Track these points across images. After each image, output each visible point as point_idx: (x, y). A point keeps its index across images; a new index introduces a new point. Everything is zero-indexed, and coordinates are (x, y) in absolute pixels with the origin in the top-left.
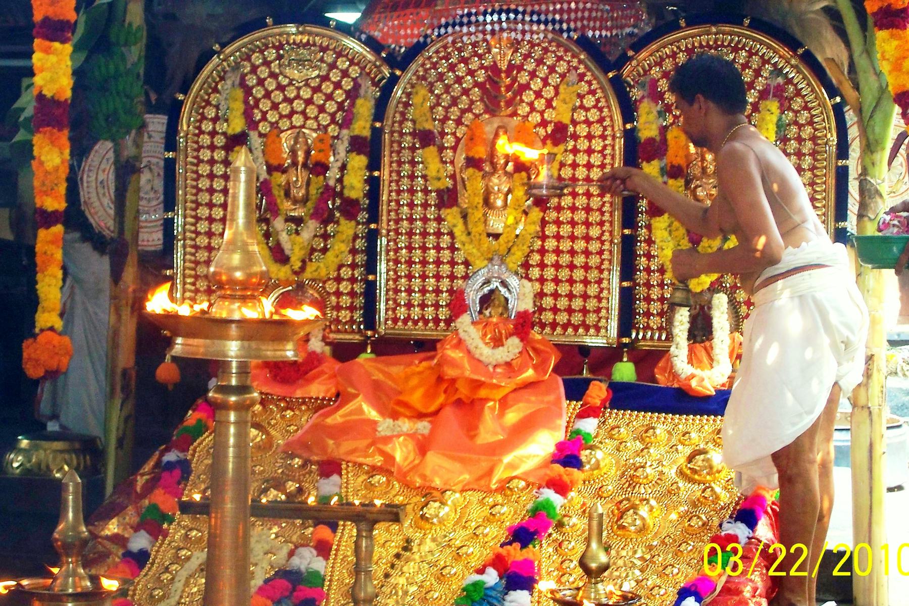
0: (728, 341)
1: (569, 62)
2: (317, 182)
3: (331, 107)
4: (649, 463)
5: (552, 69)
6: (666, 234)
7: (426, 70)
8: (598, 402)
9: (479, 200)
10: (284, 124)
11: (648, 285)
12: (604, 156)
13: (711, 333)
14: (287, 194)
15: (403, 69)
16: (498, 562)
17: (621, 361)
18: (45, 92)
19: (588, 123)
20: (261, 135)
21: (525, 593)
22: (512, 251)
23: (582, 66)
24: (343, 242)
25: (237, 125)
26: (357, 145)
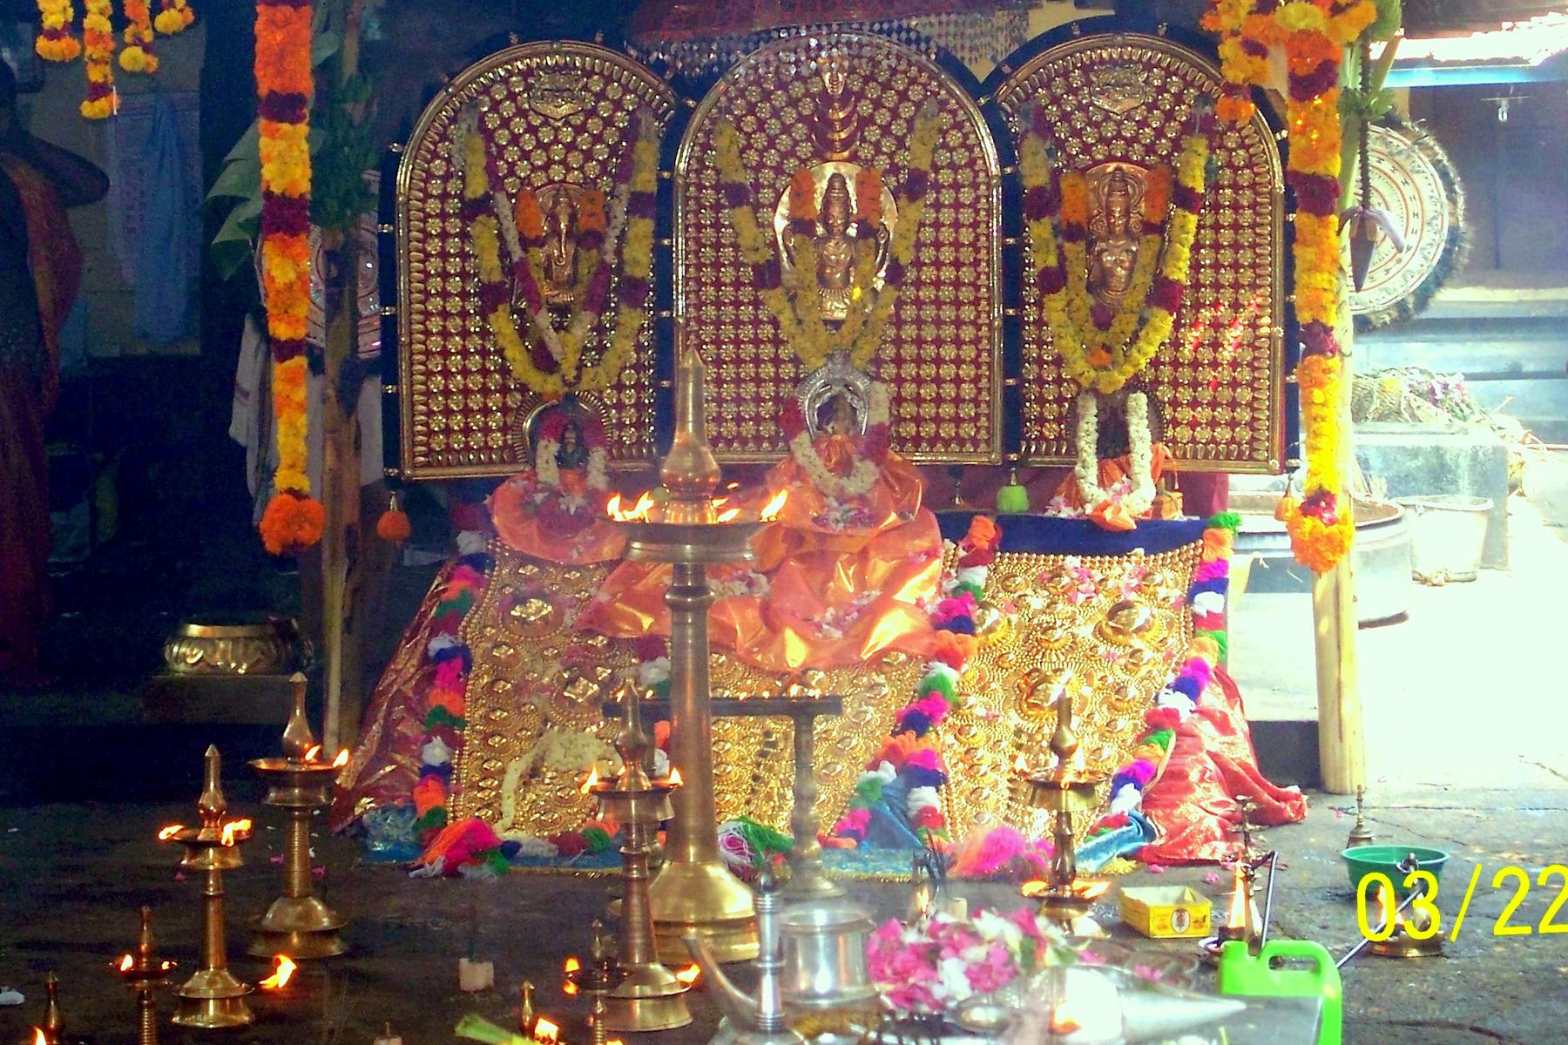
0: (1149, 456)
1: (924, 86)
2: (588, 260)
3: (601, 151)
4: (1059, 623)
5: (903, 96)
6: (1063, 317)
7: (730, 100)
8: (986, 545)
9: (812, 277)
10: (539, 179)
11: (1041, 381)
12: (977, 212)
13: (1127, 444)
14: (548, 271)
15: (698, 99)
16: (892, 754)
17: (1009, 484)
18: (273, 189)
19: (953, 166)
20: (510, 196)
21: (932, 789)
22: (859, 343)
23: (943, 92)
24: (627, 337)
25: (478, 186)
26: (638, 205)
